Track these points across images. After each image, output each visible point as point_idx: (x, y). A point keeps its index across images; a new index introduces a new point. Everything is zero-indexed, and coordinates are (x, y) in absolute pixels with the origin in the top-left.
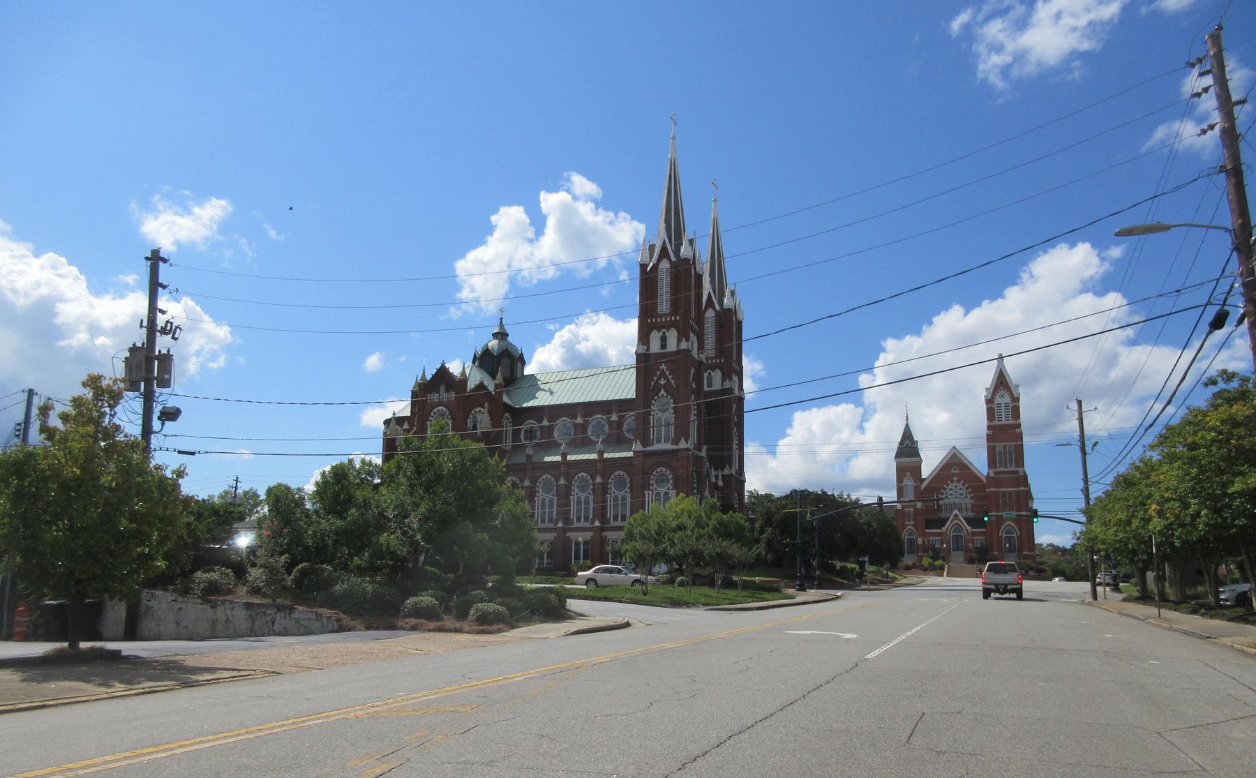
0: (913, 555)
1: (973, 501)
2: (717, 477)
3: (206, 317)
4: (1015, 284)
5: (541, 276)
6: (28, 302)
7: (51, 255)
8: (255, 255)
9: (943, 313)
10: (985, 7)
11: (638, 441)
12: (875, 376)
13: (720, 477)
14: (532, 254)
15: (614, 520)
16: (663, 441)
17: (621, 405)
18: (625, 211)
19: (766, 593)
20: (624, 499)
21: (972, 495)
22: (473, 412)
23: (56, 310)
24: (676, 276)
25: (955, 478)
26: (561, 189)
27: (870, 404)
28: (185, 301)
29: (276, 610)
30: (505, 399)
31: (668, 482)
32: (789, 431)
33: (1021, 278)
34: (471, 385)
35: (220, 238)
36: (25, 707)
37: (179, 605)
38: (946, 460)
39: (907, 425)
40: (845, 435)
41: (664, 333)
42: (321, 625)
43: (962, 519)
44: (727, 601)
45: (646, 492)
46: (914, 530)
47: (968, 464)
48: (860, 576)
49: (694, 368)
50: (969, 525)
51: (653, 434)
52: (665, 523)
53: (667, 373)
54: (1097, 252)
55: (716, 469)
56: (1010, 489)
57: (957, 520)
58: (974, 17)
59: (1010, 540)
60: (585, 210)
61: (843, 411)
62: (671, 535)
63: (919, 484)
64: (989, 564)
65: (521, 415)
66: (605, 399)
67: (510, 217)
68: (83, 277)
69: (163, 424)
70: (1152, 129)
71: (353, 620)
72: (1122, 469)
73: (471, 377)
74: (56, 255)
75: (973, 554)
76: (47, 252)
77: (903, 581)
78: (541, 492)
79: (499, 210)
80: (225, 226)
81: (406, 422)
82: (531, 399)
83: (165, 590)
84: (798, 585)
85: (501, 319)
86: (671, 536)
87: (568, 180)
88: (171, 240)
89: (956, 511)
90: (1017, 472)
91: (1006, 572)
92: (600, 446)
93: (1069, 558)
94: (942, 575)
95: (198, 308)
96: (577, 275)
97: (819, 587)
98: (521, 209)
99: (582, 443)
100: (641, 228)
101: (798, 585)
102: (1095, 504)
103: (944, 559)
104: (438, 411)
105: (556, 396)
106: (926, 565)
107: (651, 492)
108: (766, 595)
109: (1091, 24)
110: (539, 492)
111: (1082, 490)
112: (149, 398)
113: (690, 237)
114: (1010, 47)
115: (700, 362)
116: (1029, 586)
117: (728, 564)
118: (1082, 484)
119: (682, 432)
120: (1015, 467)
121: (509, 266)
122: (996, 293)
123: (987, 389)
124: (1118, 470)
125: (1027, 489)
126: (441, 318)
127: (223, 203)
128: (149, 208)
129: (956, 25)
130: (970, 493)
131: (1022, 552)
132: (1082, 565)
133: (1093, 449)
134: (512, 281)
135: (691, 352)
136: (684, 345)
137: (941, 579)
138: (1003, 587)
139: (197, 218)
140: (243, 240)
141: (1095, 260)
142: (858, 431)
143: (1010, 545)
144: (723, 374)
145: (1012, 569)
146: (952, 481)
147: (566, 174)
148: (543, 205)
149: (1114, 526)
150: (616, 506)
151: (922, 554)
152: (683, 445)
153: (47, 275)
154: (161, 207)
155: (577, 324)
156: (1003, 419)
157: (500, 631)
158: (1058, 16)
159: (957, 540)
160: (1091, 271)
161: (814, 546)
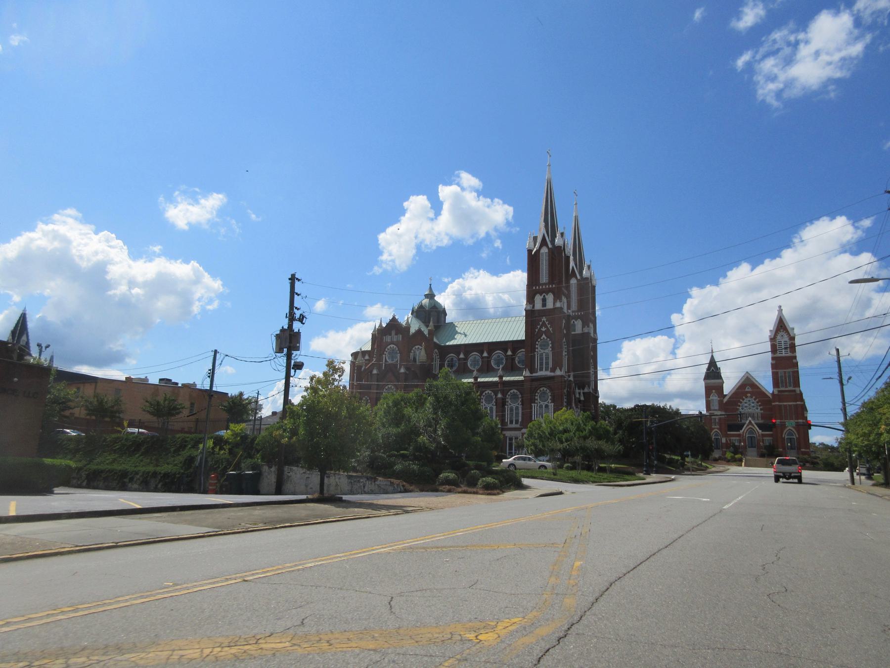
0: (719, 450)
1: (762, 411)
2: (579, 393)
3: (206, 274)
5: (439, 244)
8: (241, 231)
9: (734, 269)
11: (527, 369)
12: (683, 315)
13: (582, 394)
14: (433, 229)
15: (510, 423)
16: (544, 370)
17: (515, 345)
18: (498, 198)
19: (627, 476)
20: (517, 408)
22: (414, 349)
23: (107, 270)
25: (749, 395)
26: (453, 183)
27: (679, 335)
28: (193, 264)
29: (366, 479)
30: (435, 340)
32: (619, 355)
34: (413, 330)
35: (218, 220)
36: (170, 539)
37: (307, 476)
38: (741, 382)
41: (544, 296)
42: (393, 488)
43: (755, 425)
44: (606, 480)
45: (533, 404)
46: (719, 432)
47: (758, 385)
48: (683, 465)
50: (760, 429)
51: (537, 364)
52: (555, 427)
53: (547, 323)
54: (851, 222)
55: (579, 389)
57: (751, 426)
58: (754, 57)
59: (791, 440)
60: (471, 198)
61: (660, 341)
62: (560, 435)
63: (722, 398)
64: (778, 459)
65: (445, 351)
66: (503, 340)
67: (417, 203)
68: (125, 247)
69: (295, 372)
71: (411, 486)
72: (866, 398)
73: (412, 322)
74: (109, 233)
77: (713, 469)
79: (409, 198)
80: (222, 212)
81: (367, 355)
82: (452, 340)
83: (297, 466)
84: (645, 471)
85: (430, 285)
86: (560, 437)
87: (459, 176)
88: (186, 222)
89: (750, 419)
91: (790, 465)
92: (500, 372)
93: (836, 454)
95: (201, 268)
96: (464, 243)
97: (657, 472)
99: (487, 369)
100: (510, 209)
101: (645, 471)
102: (851, 419)
103: (742, 454)
105: (469, 337)
106: (729, 458)
108: (626, 477)
109: (843, 59)
111: (841, 410)
112: (289, 357)
114: (782, 77)
115: (569, 316)
116: (806, 474)
117: (601, 455)
118: (841, 405)
119: (557, 364)
121: (416, 237)
122: (775, 253)
123: (771, 331)
124: (864, 399)
125: (802, 403)
126: (368, 274)
127: (221, 196)
128: (171, 200)
129: (741, 62)
130: (760, 406)
131: (800, 449)
133: (848, 382)
134: (418, 247)
136: (558, 305)
137: (740, 468)
138: (788, 474)
140: (234, 222)
141: (850, 229)
143: (791, 444)
145: (792, 463)
146: (747, 397)
147: (457, 172)
149: (861, 437)
150: (512, 414)
151: (725, 450)
152: (558, 372)
153: (102, 246)
154: (179, 199)
155: (463, 278)
156: (783, 352)
157: (498, 494)
158: (817, 54)
159: (751, 439)
160: (848, 237)
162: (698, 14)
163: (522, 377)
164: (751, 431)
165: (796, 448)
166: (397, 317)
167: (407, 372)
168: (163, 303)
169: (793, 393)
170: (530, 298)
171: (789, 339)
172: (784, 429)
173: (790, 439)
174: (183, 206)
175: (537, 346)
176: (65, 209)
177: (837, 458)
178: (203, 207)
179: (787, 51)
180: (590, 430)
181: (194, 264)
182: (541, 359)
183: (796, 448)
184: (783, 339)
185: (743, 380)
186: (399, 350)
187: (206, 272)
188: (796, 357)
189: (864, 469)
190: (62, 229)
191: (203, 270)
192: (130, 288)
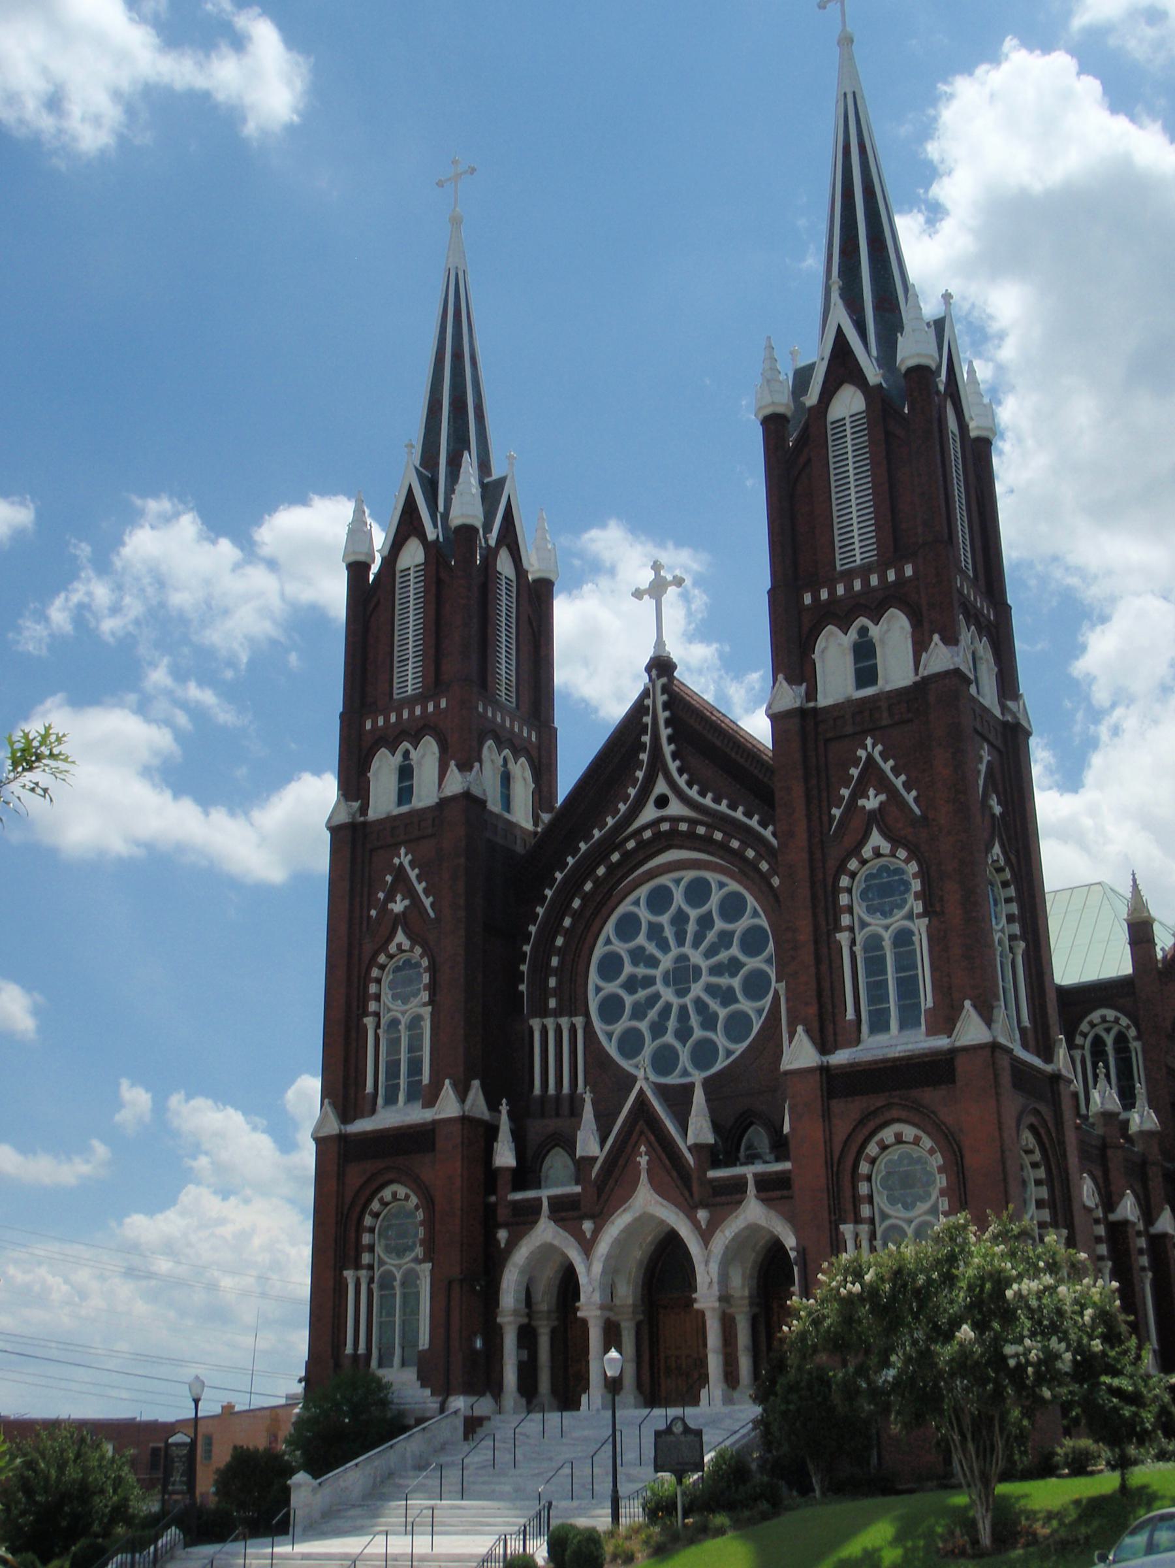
31: (930, 1182)
53: (887, 767)
107: (864, 1229)
135: (968, 682)
136: (940, 658)
163: (424, 975)
182: (876, 965)
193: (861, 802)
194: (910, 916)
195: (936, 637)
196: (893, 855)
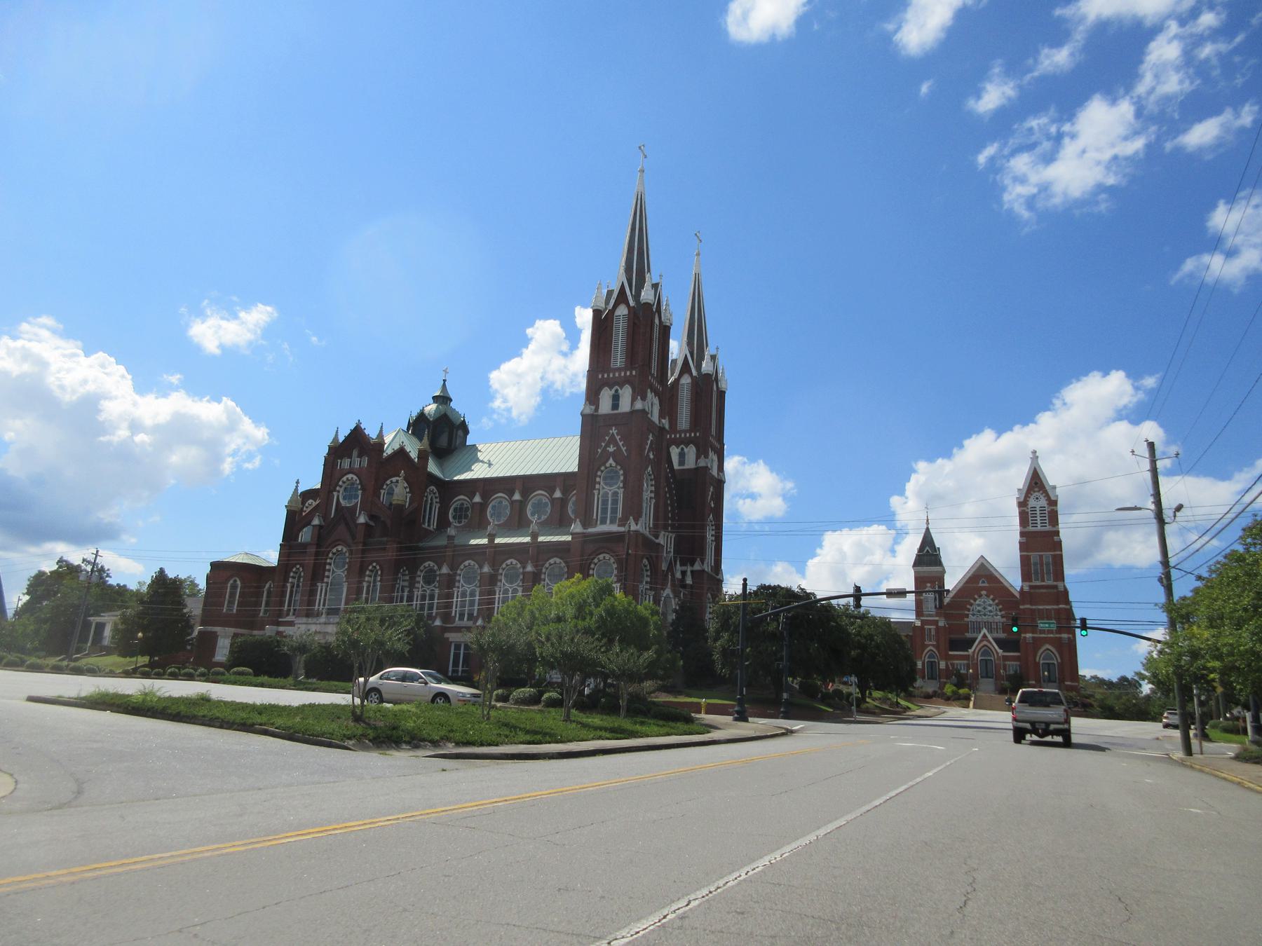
0: (934, 681)
1: (1004, 620)
2: (684, 573)
4: (1046, 409)
6: (74, 398)
7: (101, 354)
9: (974, 436)
10: (1011, 141)
13: (689, 573)
14: (566, 367)
16: (608, 522)
21: (1003, 612)
22: (388, 482)
23: (100, 407)
24: (634, 324)
25: (984, 592)
32: (818, 551)
33: (1053, 405)
35: (264, 343)
39: (928, 529)
40: (877, 557)
41: (617, 391)
43: (992, 641)
49: (653, 434)
50: (1000, 648)
51: (596, 511)
53: (618, 438)
56: (1047, 607)
57: (985, 640)
58: (1001, 150)
59: (1048, 667)
61: (875, 533)
64: (1023, 692)
65: (449, 489)
70: (1181, 261)
75: (1005, 682)
76: (96, 352)
77: (919, 712)
78: (462, 581)
80: (269, 331)
85: (445, 381)
88: (216, 343)
89: (984, 631)
90: (1056, 587)
91: (1047, 705)
94: (968, 707)
95: (238, 410)
98: (557, 322)
99: (518, 522)
101: (738, 712)
103: (970, 687)
104: (347, 479)
105: (494, 468)
109: (1115, 158)
110: (459, 581)
111: (1160, 580)
113: (713, 352)
114: (1034, 178)
116: (1081, 727)
119: (633, 509)
120: (1055, 581)
121: (542, 378)
123: (1019, 490)
125: (1068, 607)
127: (269, 309)
128: (201, 314)
129: (982, 158)
130: (1000, 610)
131: (1063, 682)
132: (1134, 701)
136: (639, 405)
137: (964, 711)
138: (1043, 726)
139: (243, 323)
140: (286, 346)
141: (1128, 387)
142: (889, 554)
143: (1049, 672)
144: (698, 450)
145: (1054, 701)
146: (980, 596)
148: (578, 320)
151: (945, 680)
154: (209, 312)
156: (1039, 525)
160: (1125, 400)
161: (781, 659)
162: (924, 89)
164: (985, 650)
165: (1057, 681)
166: (363, 426)
167: (372, 523)
168: (178, 458)
169: (1052, 591)
170: (592, 395)
171: (1048, 504)
172: (1040, 648)
173: (1048, 664)
174: (213, 321)
175: (598, 479)
176: (37, 315)
177: (1119, 698)
178: (243, 323)
179: (1046, 145)
180: (601, 616)
181: (228, 402)
182: (605, 502)
183: (1057, 681)
184: (1038, 503)
185: (974, 570)
186: (361, 483)
187: (246, 415)
188: (1058, 532)
189: (1177, 717)
190: (35, 347)
191: (241, 413)
192: (133, 434)
193: (608, 449)
194: (619, 488)
195: (639, 397)
196: (616, 467)
